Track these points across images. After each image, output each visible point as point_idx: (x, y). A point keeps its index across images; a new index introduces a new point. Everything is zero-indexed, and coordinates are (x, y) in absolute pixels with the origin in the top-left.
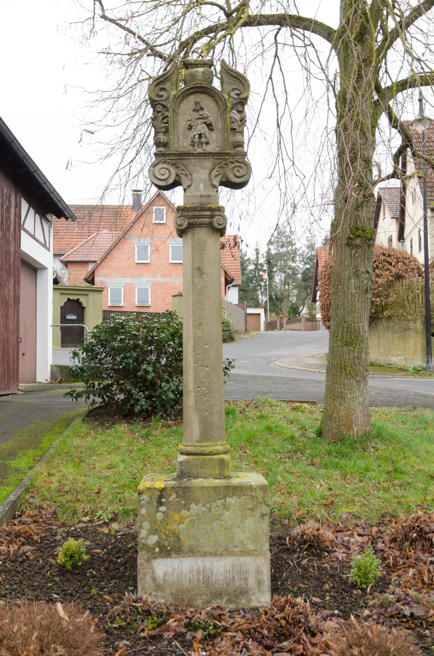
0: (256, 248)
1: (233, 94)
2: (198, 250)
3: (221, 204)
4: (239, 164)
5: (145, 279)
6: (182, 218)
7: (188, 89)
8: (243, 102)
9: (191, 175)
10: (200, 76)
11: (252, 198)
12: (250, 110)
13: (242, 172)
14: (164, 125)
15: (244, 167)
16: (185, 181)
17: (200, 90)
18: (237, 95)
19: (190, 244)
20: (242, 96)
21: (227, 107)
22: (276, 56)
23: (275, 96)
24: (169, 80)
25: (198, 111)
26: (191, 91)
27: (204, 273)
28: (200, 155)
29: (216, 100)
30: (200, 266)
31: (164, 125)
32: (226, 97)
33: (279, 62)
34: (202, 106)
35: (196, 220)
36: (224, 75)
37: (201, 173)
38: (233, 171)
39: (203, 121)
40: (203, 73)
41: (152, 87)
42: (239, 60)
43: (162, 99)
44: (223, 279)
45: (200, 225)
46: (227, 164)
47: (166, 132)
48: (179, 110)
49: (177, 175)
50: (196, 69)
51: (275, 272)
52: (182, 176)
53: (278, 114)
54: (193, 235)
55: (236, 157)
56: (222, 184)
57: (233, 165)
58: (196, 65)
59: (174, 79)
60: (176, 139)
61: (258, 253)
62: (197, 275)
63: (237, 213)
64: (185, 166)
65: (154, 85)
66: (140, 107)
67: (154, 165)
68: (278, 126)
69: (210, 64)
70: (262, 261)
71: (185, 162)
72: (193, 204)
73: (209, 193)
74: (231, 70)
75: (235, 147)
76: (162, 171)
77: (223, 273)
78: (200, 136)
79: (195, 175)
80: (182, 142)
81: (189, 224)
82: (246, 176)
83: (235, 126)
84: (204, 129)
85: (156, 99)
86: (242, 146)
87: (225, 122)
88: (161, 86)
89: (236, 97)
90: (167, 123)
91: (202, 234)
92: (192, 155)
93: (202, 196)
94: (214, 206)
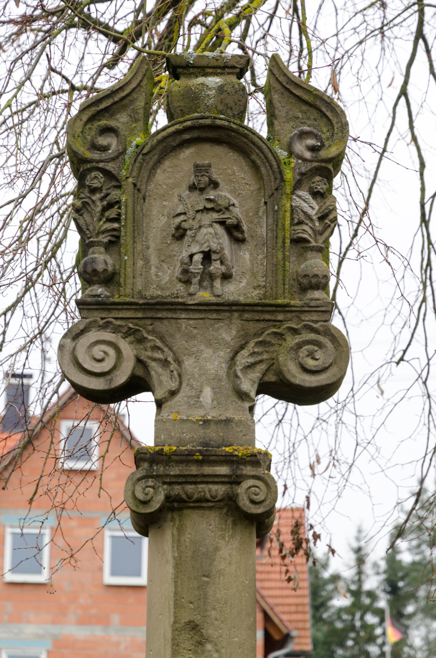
0: (355, 545)
1: (299, 148)
2: (192, 576)
3: (259, 445)
4: (312, 336)
5: (30, 630)
6: (150, 482)
7: (178, 133)
8: (328, 168)
9: (179, 362)
10: (211, 98)
11: (348, 417)
12: (345, 191)
13: (322, 358)
14: (109, 226)
15: (329, 345)
16: (163, 379)
17: (211, 134)
18: (313, 149)
19: (170, 557)
20: (324, 154)
21: (283, 180)
22: (420, 34)
23: (414, 139)
24: (125, 107)
25: (202, 190)
26: (187, 136)
27: (208, 640)
28: (205, 307)
29: (253, 162)
30: (197, 618)
31: (109, 226)
32: (283, 154)
33: (428, 51)
34: (215, 176)
35: (190, 488)
36: (276, 97)
37: (206, 357)
38: (295, 348)
39: (215, 216)
40: (221, 89)
41: (79, 124)
42: (320, 59)
43: (104, 156)
44: (260, 635)
45: (201, 504)
46: (280, 336)
47: (114, 243)
48: (152, 186)
49: (139, 361)
50: (201, 80)
51: (411, 616)
52: (153, 364)
53: (423, 190)
54: (181, 530)
55: (306, 317)
56: (264, 388)
57: (298, 339)
58: (201, 69)
59: (140, 103)
60: (140, 263)
61: (360, 561)
62: (187, 645)
63: (304, 457)
64: (162, 338)
65: (85, 118)
66: (42, 170)
67: (74, 334)
68: (425, 221)
69: (242, 66)
70: (372, 583)
71: (162, 327)
72: (180, 443)
73: (229, 415)
74: (297, 86)
75: (304, 289)
76: (98, 352)
77: (260, 616)
78: (207, 256)
79: (189, 363)
80: (156, 271)
81: (168, 498)
82: (334, 370)
83: (306, 231)
84: (220, 240)
85: (88, 155)
86: (324, 287)
87: (276, 221)
88: (103, 122)
89: (308, 155)
90: (117, 220)
91: (204, 528)
92: (184, 307)
93: (206, 422)
94: (240, 451)
